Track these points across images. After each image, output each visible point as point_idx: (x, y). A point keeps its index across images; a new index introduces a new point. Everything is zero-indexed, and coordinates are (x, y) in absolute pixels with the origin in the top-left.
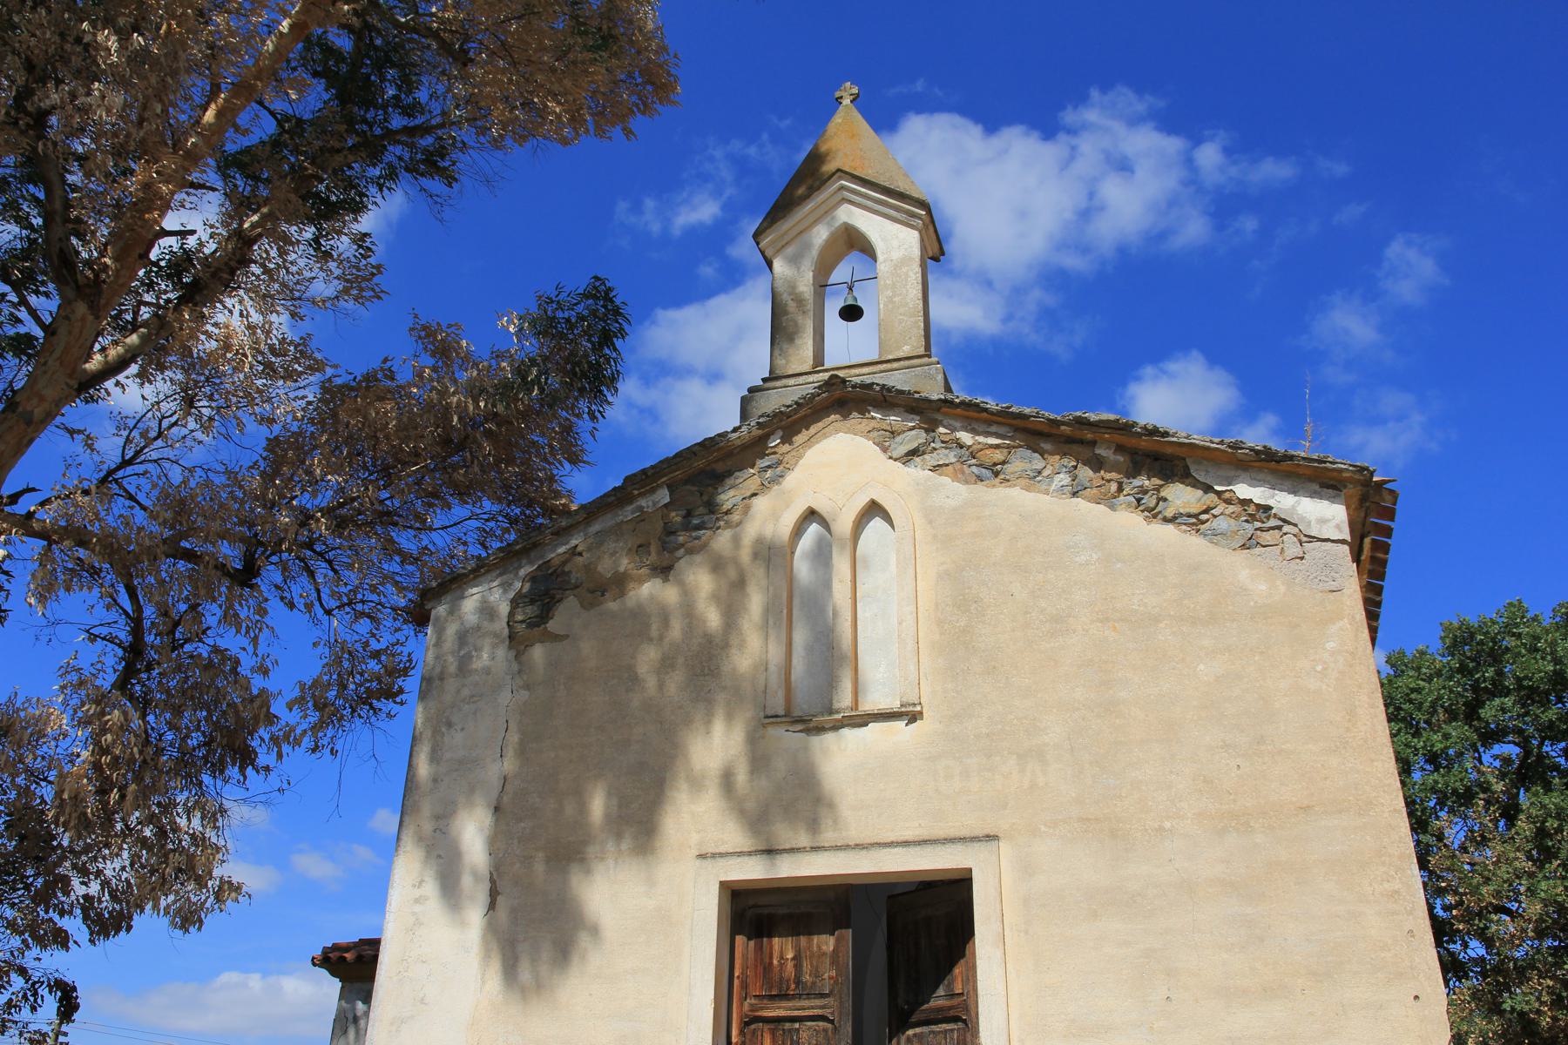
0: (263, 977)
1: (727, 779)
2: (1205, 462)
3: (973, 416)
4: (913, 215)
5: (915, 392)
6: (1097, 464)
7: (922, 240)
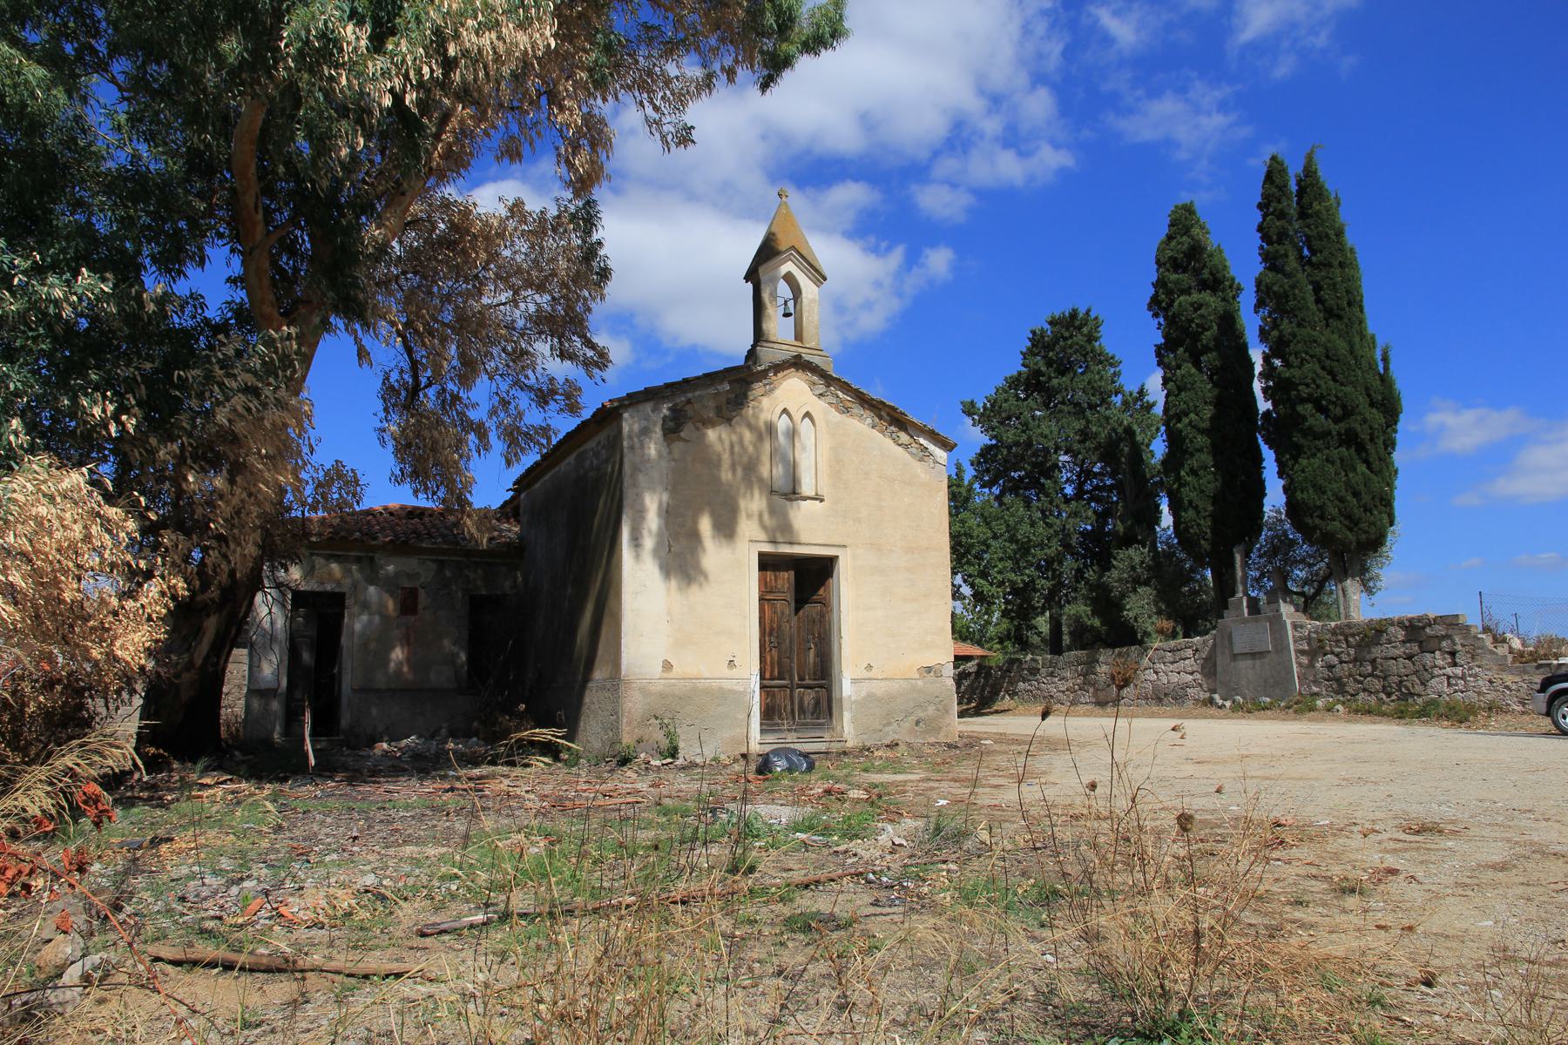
0: (1227, 608)
1: (760, 516)
3: (846, 387)
6: (881, 418)
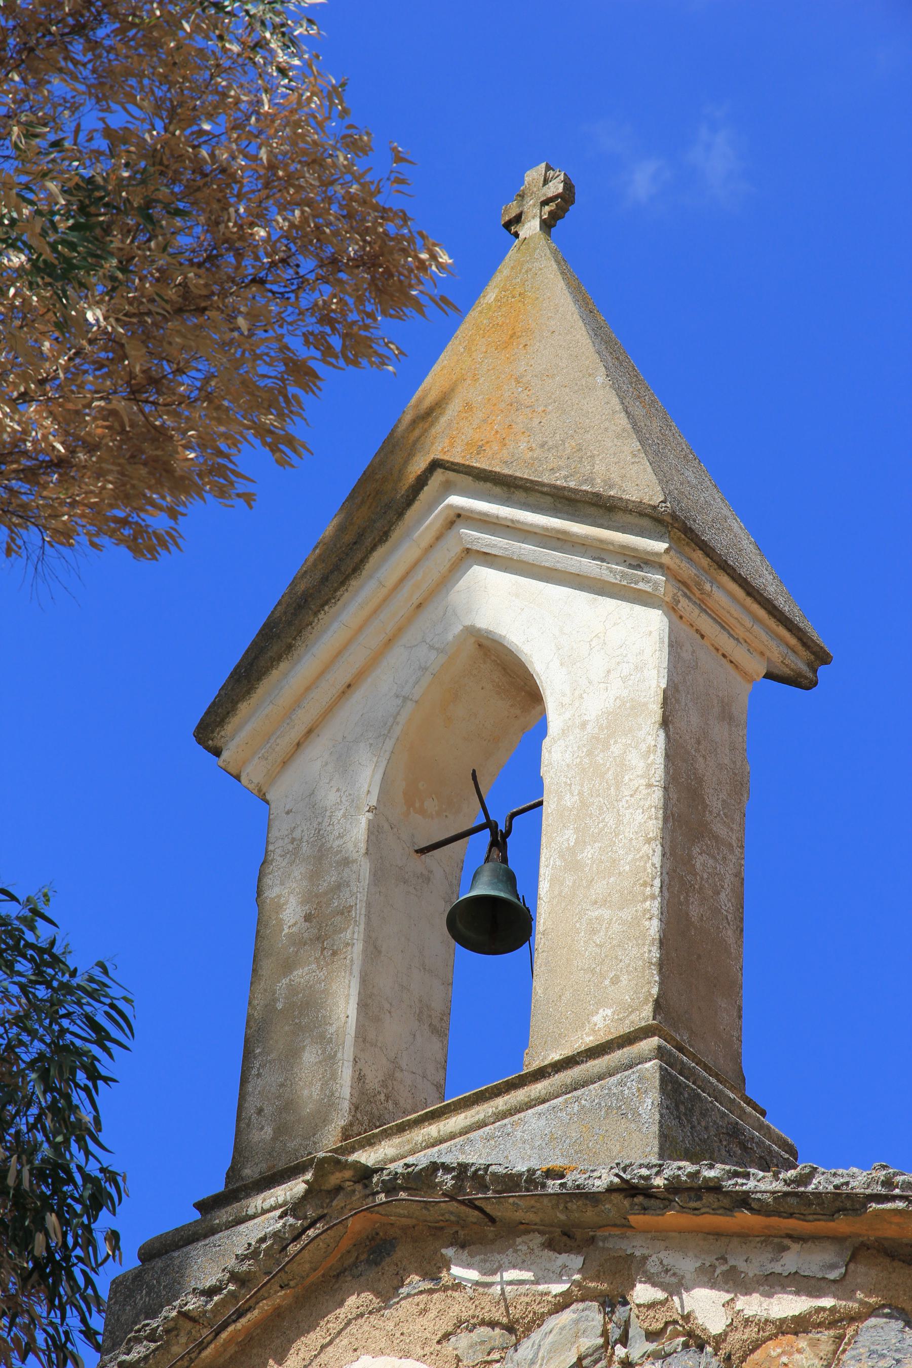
2: (795, 1247)
4: (641, 561)
5: (550, 1174)
7: (675, 645)
